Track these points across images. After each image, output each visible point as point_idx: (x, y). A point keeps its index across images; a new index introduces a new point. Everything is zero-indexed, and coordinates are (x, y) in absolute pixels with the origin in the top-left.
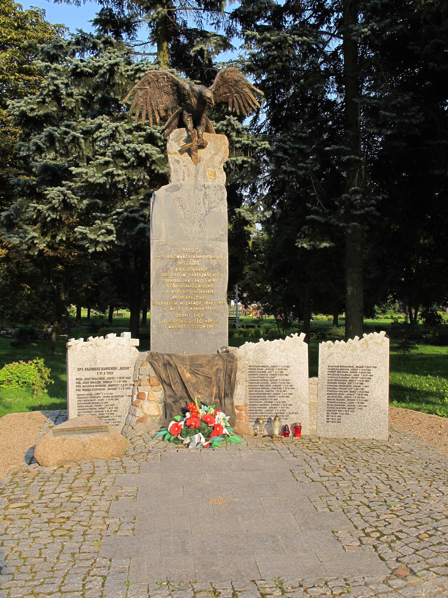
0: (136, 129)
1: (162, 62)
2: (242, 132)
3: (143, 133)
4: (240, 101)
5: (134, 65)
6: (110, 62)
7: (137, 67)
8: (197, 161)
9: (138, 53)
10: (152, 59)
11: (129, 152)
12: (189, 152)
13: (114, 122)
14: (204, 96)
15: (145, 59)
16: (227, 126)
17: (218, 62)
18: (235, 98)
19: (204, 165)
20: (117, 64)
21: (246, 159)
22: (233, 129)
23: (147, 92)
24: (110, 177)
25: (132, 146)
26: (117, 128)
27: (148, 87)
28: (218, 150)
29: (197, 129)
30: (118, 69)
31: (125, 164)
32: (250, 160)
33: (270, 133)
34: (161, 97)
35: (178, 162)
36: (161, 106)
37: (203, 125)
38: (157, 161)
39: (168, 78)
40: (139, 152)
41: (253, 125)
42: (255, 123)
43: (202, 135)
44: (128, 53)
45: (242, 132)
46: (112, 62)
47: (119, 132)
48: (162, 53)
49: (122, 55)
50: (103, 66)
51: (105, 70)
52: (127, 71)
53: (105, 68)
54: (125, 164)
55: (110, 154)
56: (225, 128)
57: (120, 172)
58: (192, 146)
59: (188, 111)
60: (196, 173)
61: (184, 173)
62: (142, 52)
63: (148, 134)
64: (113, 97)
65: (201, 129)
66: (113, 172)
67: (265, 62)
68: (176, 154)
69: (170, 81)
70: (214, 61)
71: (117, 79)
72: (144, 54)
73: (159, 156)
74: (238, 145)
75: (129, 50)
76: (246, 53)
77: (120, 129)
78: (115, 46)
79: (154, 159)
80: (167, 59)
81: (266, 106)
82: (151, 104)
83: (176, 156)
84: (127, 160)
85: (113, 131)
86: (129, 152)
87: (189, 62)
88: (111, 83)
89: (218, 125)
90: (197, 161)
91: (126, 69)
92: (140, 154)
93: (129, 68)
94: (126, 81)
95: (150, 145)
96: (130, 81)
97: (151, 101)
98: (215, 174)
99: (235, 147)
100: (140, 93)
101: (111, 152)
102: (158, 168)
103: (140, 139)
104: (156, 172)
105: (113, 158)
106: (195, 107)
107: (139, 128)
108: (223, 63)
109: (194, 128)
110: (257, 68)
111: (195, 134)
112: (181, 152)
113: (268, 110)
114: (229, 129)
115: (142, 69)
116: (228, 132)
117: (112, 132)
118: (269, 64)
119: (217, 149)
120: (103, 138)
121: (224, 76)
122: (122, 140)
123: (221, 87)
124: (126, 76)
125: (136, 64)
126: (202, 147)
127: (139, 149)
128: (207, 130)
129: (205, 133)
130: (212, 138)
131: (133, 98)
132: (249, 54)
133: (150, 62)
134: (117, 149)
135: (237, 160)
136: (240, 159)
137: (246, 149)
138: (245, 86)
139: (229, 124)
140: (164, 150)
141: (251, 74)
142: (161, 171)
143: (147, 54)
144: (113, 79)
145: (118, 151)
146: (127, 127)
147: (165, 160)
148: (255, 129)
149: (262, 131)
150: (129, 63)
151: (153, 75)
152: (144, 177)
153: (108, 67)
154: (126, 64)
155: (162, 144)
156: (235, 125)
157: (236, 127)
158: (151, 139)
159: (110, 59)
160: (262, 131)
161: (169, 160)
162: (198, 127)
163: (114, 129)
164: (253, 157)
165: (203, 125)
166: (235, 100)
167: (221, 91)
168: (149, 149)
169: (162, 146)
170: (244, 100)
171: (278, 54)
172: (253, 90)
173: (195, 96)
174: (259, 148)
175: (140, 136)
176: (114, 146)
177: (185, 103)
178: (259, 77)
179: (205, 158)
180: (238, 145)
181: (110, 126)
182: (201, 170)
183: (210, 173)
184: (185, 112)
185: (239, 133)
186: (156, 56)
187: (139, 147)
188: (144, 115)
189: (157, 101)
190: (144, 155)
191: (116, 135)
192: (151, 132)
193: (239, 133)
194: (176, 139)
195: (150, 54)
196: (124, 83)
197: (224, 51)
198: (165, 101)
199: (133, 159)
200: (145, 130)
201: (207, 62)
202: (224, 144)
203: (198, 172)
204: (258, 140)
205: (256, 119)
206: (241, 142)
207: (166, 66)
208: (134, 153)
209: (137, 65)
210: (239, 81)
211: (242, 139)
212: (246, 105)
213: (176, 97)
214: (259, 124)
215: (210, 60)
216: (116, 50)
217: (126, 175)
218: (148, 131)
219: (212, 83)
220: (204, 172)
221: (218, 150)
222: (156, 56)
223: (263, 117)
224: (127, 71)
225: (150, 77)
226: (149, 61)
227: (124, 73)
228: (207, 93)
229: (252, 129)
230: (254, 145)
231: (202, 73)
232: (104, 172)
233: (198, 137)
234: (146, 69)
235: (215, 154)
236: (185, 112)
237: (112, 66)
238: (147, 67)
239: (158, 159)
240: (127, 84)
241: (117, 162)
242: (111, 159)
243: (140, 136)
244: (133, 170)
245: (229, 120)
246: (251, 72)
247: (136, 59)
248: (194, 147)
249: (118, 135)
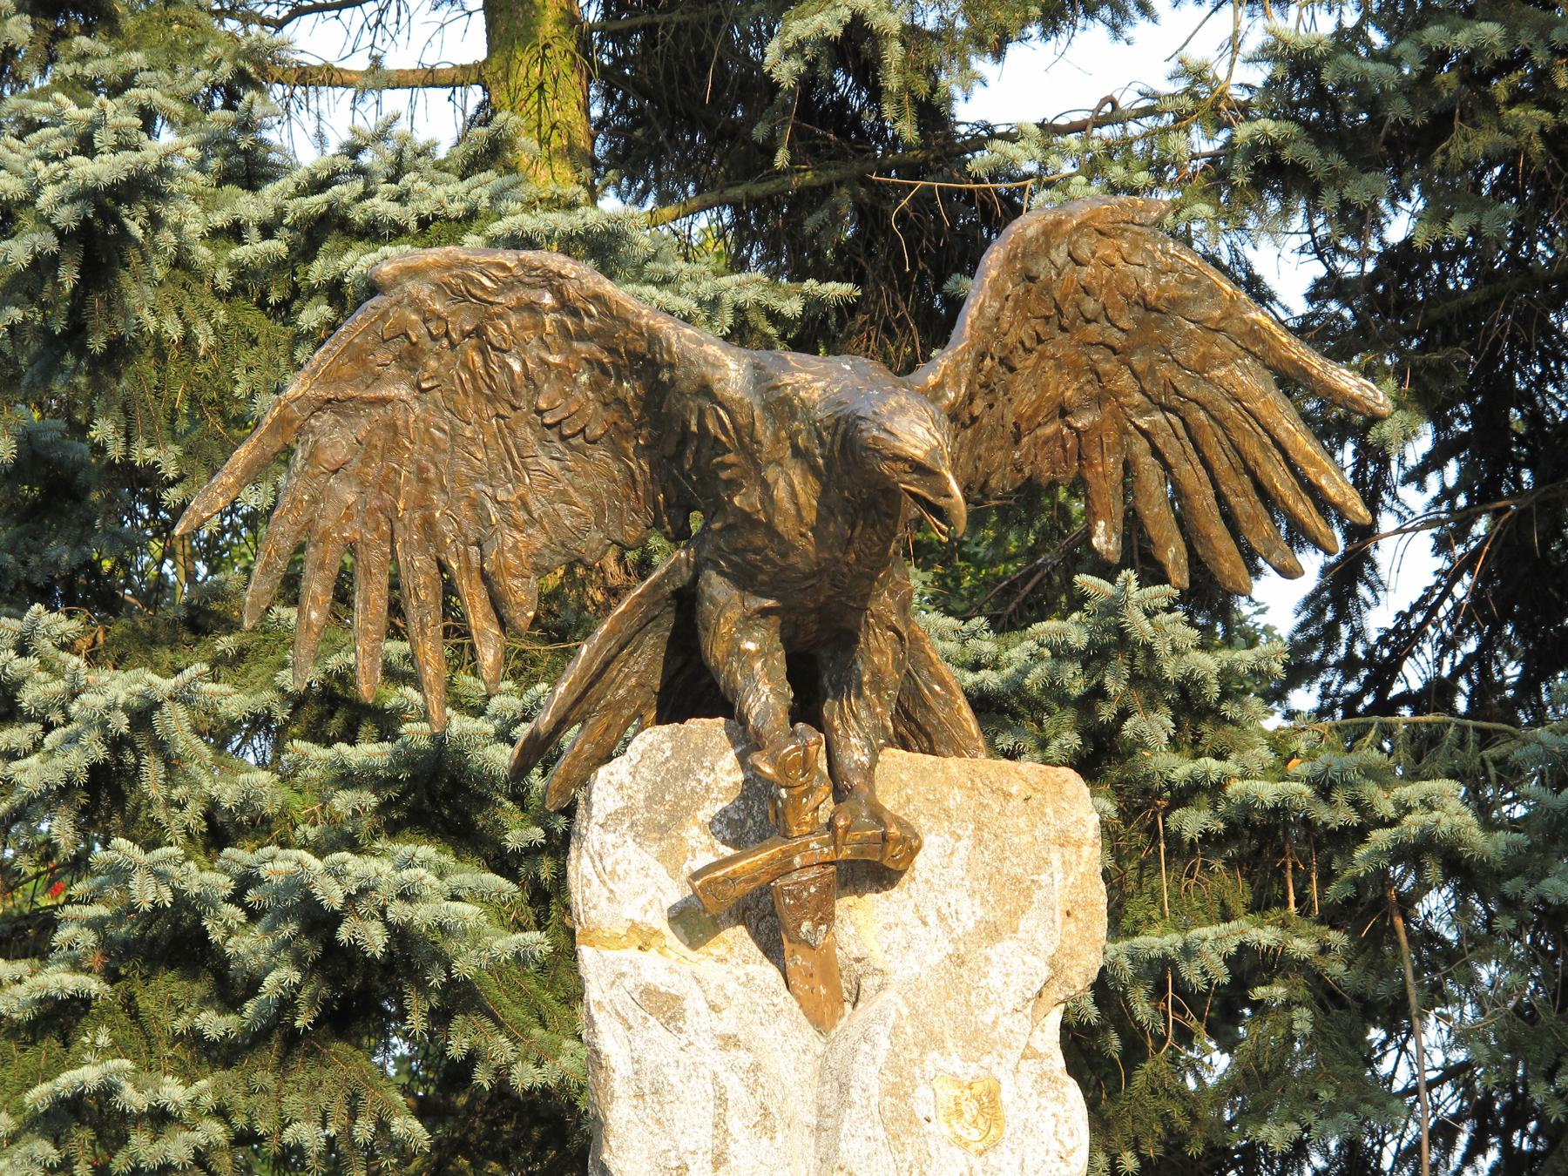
0: (310, 712)
1: (527, 144)
2: (1230, 709)
3: (368, 752)
4: (1192, 475)
5: (286, 184)
6: (85, 169)
7: (316, 203)
8: (828, 994)
9: (329, 77)
10: (438, 121)
11: (253, 915)
12: (766, 918)
13: (120, 662)
14: (876, 451)
15: (381, 136)
16: (1093, 658)
17: (1001, 119)
18: (1141, 446)
19: (896, 1031)
20: (144, 187)
21: (1265, 936)
22: (1148, 681)
23: (392, 427)
24: (84, 1135)
25: (278, 864)
26: (143, 715)
27: (402, 391)
28: (1012, 894)
29: (818, 723)
30: (155, 221)
31: (214, 1024)
32: (1302, 946)
33: (1485, 690)
34: (515, 462)
35: (663, 1006)
36: (510, 537)
37: (878, 685)
38: (493, 991)
39: (565, 305)
40: (336, 919)
41: (1331, 634)
42: (1343, 615)
43: (869, 773)
44: (242, 78)
45: (1230, 709)
46: (105, 168)
47: (161, 747)
48: (526, 69)
49: (190, 100)
50: (28, 202)
51: (49, 243)
52: (236, 232)
53: (44, 220)
54: (214, 1024)
55: (89, 938)
56: (1075, 681)
57: (173, 1092)
58: (786, 869)
59: (744, 579)
60: (830, 1097)
61: (721, 1100)
62: (360, 63)
63: (407, 759)
64: (115, 452)
65: (856, 729)
66: (107, 1091)
67: (1398, 110)
68: (644, 939)
69: (582, 336)
70: (967, 112)
71: (146, 306)
72: (378, 78)
73: (506, 943)
74: (1193, 821)
75: (251, 53)
76: (1235, 42)
77: (175, 723)
78: (129, 24)
79: (464, 967)
80: (568, 113)
81: (1434, 461)
82: (428, 524)
83: (651, 958)
84: (231, 989)
85: (117, 744)
86: (253, 915)
87: (759, 132)
88: (97, 344)
89: (1019, 651)
90: (828, 994)
91: (220, 219)
92: (343, 934)
93: (249, 206)
94: (221, 315)
95: (427, 851)
96: (255, 320)
97: (424, 504)
98: (990, 1105)
99: (1174, 839)
100: (337, 439)
101: (96, 924)
102: (501, 1047)
103: (343, 801)
104: (482, 1077)
105: (112, 976)
106: (807, 544)
107: (334, 709)
108: (1048, 129)
109: (796, 715)
110: (1337, 161)
111: (806, 764)
112: (695, 922)
113: (1447, 494)
114: (1113, 686)
115: (357, 215)
116: (1107, 713)
117: (100, 753)
118: (1440, 126)
119: (1002, 886)
120: (31, 801)
121: (1041, 269)
122: (192, 815)
123: (1024, 363)
124: (224, 278)
125: (300, 175)
126: (874, 869)
127: (332, 895)
128: (915, 729)
129: (893, 757)
130: (956, 798)
131: (285, 473)
132: (1267, 53)
133: (424, 152)
134: (146, 893)
135: (1188, 952)
136: (1213, 944)
137: (1264, 850)
138: (1221, 346)
139: (1113, 643)
140: (547, 900)
141: (1286, 212)
142: (525, 1077)
143: (402, 81)
144: (115, 304)
145: (157, 910)
146: (233, 701)
147: (558, 979)
148: (1349, 666)
149: (1413, 675)
150: (250, 170)
151: (441, 288)
152: (382, 1126)
153: (66, 216)
154: (225, 178)
155: (537, 834)
156: (1162, 647)
157: (1171, 670)
158: (437, 800)
159: (86, 146)
160: (1413, 675)
161: (593, 992)
162: (830, 709)
163: (121, 723)
164: (1333, 917)
165: (878, 685)
166: (1147, 462)
167: (1025, 397)
168: (426, 887)
169: (532, 851)
170: (1221, 464)
171: (1511, 36)
172: (1289, 380)
173: (797, 452)
174: (1380, 837)
175: (347, 778)
176: (120, 874)
177: (716, 508)
178: (1359, 220)
179: (902, 969)
180: (1193, 821)
181: (92, 701)
182: (868, 1077)
183: (947, 1092)
184: (717, 587)
185: (1194, 710)
186: (476, 95)
187: (338, 874)
188: (371, 599)
189: (475, 505)
190: (375, 940)
191: (134, 775)
192: (438, 740)
193: (1194, 710)
194: (645, 826)
195: (430, 78)
196: (205, 338)
197: (1045, 35)
198: (551, 499)
199: (281, 977)
200: (386, 723)
201: (908, 130)
202: (1063, 840)
203: (844, 1088)
204: (1370, 773)
205: (1348, 578)
206: (1218, 788)
207: (563, 170)
208: (289, 929)
209: (318, 185)
210: (1175, 303)
211: (1230, 766)
212: (1245, 504)
213: (641, 467)
214: (1378, 619)
215: (933, 115)
216: (137, 58)
217: (221, 1113)
218: (416, 733)
219: (938, 329)
220: (899, 1091)
221: (1012, 894)
222: (476, 95)
223: (1408, 567)
224: (236, 232)
225: (416, 304)
226: (421, 139)
227: (202, 253)
228: (900, 425)
229: (1321, 666)
230: (1342, 815)
231: (870, 216)
232: (39, 1095)
233: (840, 792)
234: (394, 210)
235: (992, 932)
236: (717, 587)
237: (105, 203)
238: (401, 198)
239: (497, 969)
240: (232, 340)
241: (146, 1002)
242: (94, 985)
243: (347, 778)
244: (283, 1066)
245: (1113, 608)
246: (1285, 195)
247: (306, 135)
248: (805, 878)
249: (152, 768)
